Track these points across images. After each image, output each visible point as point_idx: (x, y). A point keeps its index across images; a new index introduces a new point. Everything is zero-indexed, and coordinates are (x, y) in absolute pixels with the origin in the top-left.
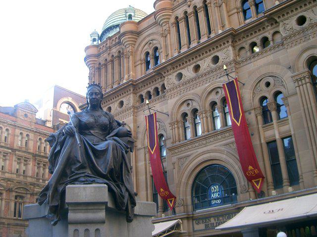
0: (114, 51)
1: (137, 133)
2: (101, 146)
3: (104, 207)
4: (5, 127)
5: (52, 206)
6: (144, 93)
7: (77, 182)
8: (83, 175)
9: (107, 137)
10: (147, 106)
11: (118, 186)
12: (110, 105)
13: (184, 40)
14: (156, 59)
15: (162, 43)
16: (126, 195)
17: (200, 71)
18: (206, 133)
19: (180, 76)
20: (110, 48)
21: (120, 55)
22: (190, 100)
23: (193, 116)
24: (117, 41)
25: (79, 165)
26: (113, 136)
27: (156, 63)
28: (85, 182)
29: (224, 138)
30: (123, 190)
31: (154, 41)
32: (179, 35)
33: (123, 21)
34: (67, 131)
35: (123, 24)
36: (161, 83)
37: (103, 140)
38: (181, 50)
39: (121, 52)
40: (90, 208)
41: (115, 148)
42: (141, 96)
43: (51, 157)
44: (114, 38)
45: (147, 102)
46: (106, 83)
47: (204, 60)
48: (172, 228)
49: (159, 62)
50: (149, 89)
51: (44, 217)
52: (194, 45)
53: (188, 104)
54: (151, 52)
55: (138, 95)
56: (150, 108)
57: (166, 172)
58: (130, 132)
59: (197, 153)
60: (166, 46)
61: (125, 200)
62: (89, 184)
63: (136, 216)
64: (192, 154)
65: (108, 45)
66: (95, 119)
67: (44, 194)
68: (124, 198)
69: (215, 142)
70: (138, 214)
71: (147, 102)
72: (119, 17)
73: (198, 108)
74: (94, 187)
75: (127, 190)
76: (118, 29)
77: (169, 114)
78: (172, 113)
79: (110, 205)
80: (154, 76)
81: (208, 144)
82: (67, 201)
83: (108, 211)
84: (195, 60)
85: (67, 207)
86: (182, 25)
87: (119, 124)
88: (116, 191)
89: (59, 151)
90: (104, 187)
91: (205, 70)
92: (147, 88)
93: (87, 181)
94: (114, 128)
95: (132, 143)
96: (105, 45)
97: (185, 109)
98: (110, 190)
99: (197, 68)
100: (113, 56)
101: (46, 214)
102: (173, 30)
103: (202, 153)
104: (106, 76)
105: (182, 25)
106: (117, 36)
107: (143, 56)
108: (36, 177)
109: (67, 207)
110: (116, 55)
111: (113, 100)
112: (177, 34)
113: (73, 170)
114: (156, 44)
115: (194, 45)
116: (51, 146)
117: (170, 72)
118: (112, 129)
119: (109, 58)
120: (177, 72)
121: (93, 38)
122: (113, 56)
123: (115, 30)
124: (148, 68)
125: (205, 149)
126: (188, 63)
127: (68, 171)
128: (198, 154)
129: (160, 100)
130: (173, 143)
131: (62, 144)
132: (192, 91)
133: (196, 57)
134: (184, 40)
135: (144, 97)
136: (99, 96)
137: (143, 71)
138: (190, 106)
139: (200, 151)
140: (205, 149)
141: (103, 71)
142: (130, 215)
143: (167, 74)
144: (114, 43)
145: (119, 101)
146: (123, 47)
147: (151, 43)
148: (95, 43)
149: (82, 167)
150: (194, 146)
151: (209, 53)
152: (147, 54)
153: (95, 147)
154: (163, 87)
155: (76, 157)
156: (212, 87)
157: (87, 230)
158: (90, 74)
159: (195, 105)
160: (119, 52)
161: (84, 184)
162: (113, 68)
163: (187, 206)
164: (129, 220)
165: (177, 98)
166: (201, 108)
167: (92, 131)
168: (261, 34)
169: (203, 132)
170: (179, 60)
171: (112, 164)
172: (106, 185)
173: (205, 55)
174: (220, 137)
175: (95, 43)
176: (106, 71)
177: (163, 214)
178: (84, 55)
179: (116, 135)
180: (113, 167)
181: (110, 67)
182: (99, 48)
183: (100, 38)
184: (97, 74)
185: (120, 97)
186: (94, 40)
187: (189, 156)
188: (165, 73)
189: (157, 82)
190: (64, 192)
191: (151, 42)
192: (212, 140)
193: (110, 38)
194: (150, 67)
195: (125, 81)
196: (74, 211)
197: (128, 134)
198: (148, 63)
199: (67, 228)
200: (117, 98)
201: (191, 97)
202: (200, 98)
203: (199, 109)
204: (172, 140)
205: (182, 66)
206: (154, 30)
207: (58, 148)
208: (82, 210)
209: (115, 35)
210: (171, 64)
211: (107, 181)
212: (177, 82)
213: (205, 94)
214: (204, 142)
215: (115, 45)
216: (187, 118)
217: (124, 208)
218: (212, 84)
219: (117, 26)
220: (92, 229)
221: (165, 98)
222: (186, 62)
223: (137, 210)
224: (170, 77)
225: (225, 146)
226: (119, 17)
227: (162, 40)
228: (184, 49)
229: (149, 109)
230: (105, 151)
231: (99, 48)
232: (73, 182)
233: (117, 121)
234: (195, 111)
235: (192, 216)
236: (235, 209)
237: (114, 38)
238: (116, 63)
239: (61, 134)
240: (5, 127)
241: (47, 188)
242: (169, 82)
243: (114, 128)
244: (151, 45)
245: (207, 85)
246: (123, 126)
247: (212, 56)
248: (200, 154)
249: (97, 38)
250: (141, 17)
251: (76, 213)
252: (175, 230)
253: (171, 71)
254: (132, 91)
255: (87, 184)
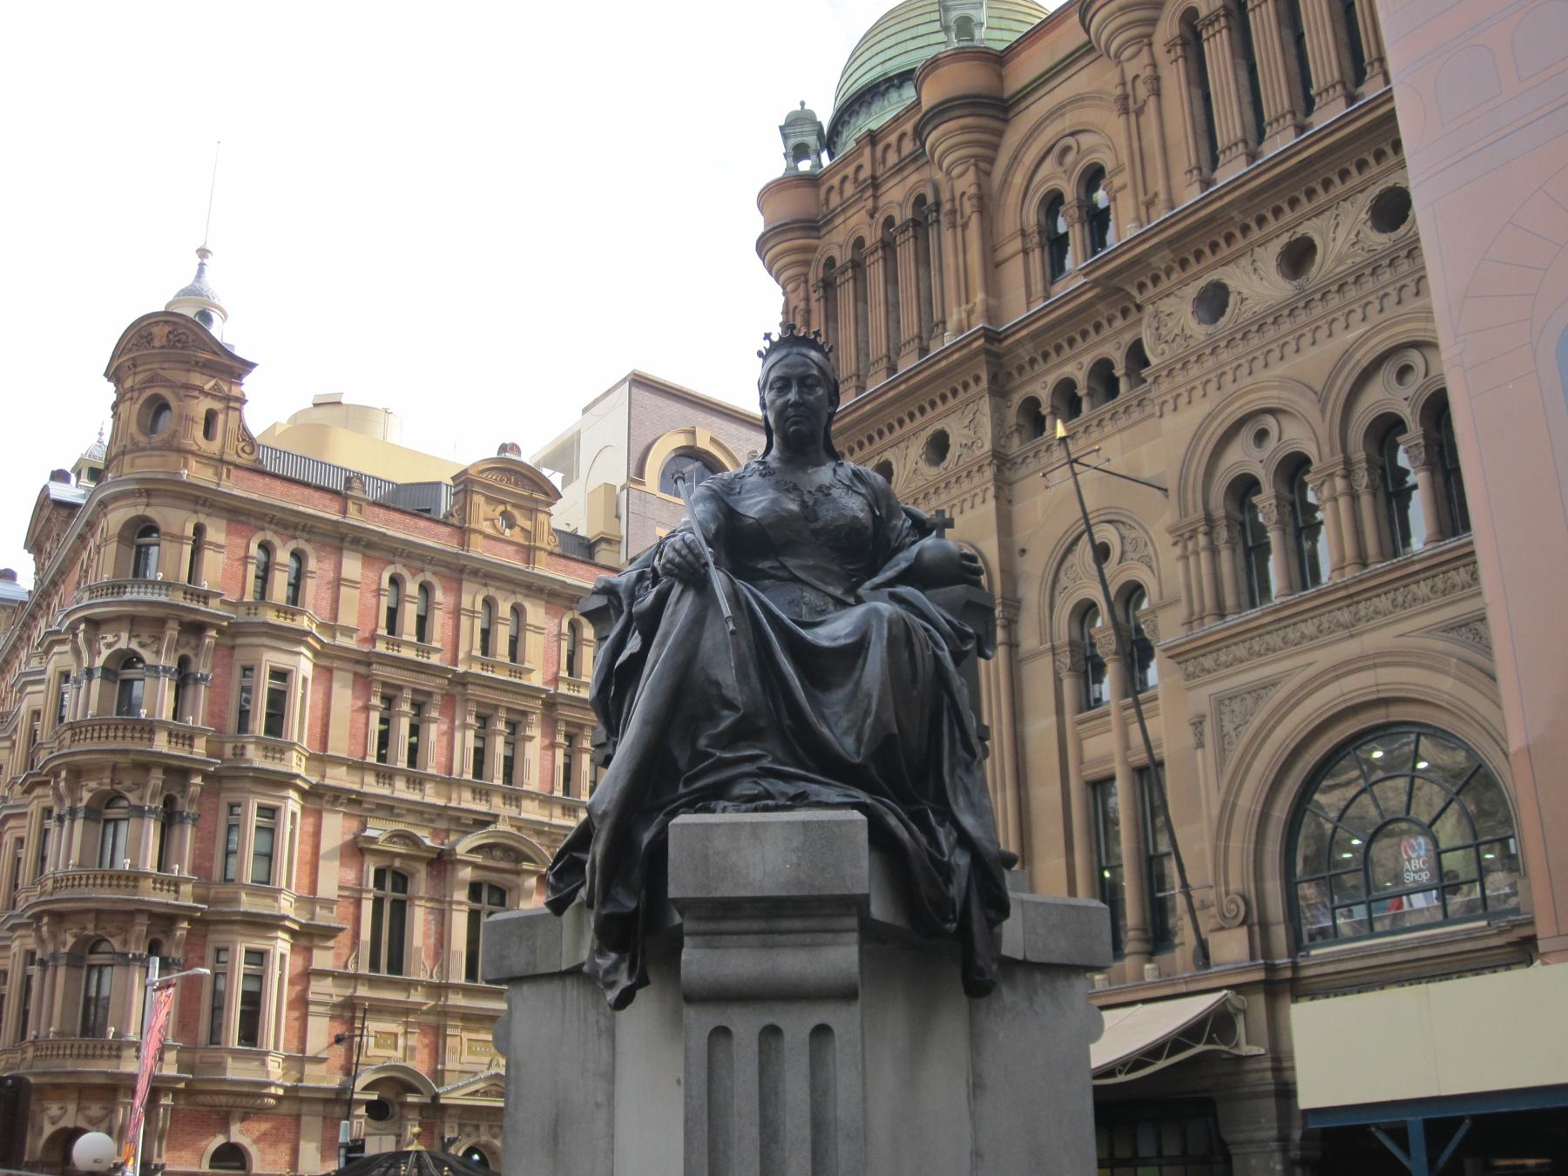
0: (896, 196)
1: (1010, 575)
2: (836, 630)
3: (853, 922)
4: (414, 575)
5: (607, 916)
6: (1042, 389)
7: (722, 804)
8: (747, 768)
9: (861, 591)
10: (1059, 454)
11: (920, 820)
12: (889, 455)
13: (1230, 123)
14: (1097, 221)
15: (1121, 141)
16: (962, 860)
17: (1314, 269)
18: (1351, 573)
19: (1214, 301)
20: (875, 184)
21: (924, 217)
22: (1272, 411)
23: (1286, 493)
24: (908, 146)
25: (728, 719)
26: (891, 583)
27: (1098, 240)
28: (754, 802)
29: (1444, 593)
30: (944, 836)
31: (1082, 138)
32: (1207, 98)
33: (930, 53)
34: (670, 561)
35: (934, 64)
36: (1127, 338)
37: (841, 604)
38: (1218, 174)
39: (930, 199)
40: (786, 924)
41: (901, 639)
42: (1031, 405)
43: (603, 688)
44: (893, 138)
45: (1060, 431)
46: (862, 349)
47: (1333, 211)
48: (1191, 1033)
49: (1111, 238)
50: (1069, 370)
51: (575, 972)
52: (1280, 141)
53: (1261, 436)
54: (1070, 192)
55: (1017, 399)
56: (1075, 461)
57: (1160, 764)
58: (973, 559)
59: (1311, 671)
60: (1140, 158)
61: (956, 890)
62: (778, 808)
63: (1012, 966)
64: (1289, 673)
65: (866, 173)
66: (804, 504)
67: (568, 866)
68: (948, 880)
69: (1400, 613)
70: (1020, 957)
71: (1060, 431)
72: (914, 32)
73: (1311, 450)
74: (806, 825)
75: (964, 840)
76: (909, 93)
77: (1171, 484)
78: (1182, 477)
79: (879, 910)
80: (1090, 304)
81: (1362, 626)
82: (673, 892)
83: (870, 932)
84: (1288, 216)
85: (677, 919)
86: (1218, 50)
87: (921, 527)
88: (905, 835)
89: (639, 659)
90: (851, 822)
91: (1340, 260)
92: (1062, 364)
93: (769, 796)
94: (895, 544)
95: (980, 611)
96: (850, 171)
97: (1243, 457)
98: (880, 836)
99: (1298, 257)
100: (889, 222)
101: (585, 955)
102: (1174, 77)
103: (1334, 667)
104: (861, 320)
105: (1218, 50)
106: (908, 127)
107: (1032, 216)
108: (558, 793)
109: (677, 919)
110: (902, 215)
111: (898, 432)
112: (1197, 93)
113: (702, 742)
114: (1091, 150)
115: (1280, 141)
116: (601, 639)
117: (1165, 284)
118: (888, 551)
119: (872, 236)
120: (1202, 283)
121: (793, 142)
122: (889, 222)
123: (893, 95)
124: (1056, 268)
125: (1350, 648)
126: (1256, 234)
127: (682, 757)
128: (1316, 677)
129: (1122, 422)
130: (1189, 623)
131: (649, 623)
132: (1279, 370)
133: (1294, 203)
134: (1230, 123)
135: (1045, 410)
136: (820, 391)
137: (1038, 287)
138: (1271, 443)
139: (1324, 657)
140: (1350, 648)
141: (846, 294)
142: (980, 963)
143: (1151, 290)
144: (892, 158)
145: (929, 431)
146: (939, 176)
147: (1067, 149)
148: (805, 166)
149: (743, 732)
150: (1292, 635)
151: (1355, 179)
152: (1053, 202)
153: (807, 634)
154: (1137, 357)
155: (717, 684)
156: (1378, 344)
157: (722, 1032)
158: (786, 312)
159: (1295, 436)
160: (920, 200)
161: (756, 810)
162: (891, 279)
163: (1265, 926)
164: (978, 988)
165: (1202, 408)
166: (1326, 449)
167: (791, 563)
168: (1057, 366)
169: (1339, 568)
170: (1211, 218)
171: (889, 715)
172: (857, 815)
173: (1338, 188)
174: (1423, 589)
175: (805, 166)
176: (861, 297)
177: (1147, 966)
178: (757, 225)
179: (914, 575)
180: (895, 730)
181: (876, 273)
182: (823, 190)
183: (829, 141)
184: (817, 308)
185: (930, 414)
186: (799, 152)
187: (1271, 684)
188: (1142, 287)
189: (1106, 331)
190: (660, 847)
191: (1070, 141)
192: (1383, 603)
193: (873, 138)
194: (1069, 262)
195: (949, 340)
196: (711, 938)
197: (964, 569)
198: (1057, 246)
199: (264, 1063)
200: (919, 420)
201: (1271, 398)
202: (1322, 400)
203: (1313, 455)
204: (1181, 612)
205: (1225, 251)
206: (1080, 81)
207: (634, 644)
208: (747, 933)
209: (896, 119)
210: (1169, 242)
211: (863, 797)
212: (1199, 331)
213: (1344, 383)
214: (1345, 616)
215: (899, 169)
216: (1255, 499)
217: (952, 927)
218: (1376, 330)
219: (905, 77)
220: (796, 1024)
221: (1148, 410)
222: (1245, 229)
223: (1014, 937)
224: (1166, 305)
225: (1453, 635)
226: (914, 32)
227: (1115, 124)
228: (1231, 170)
229: (1072, 462)
230: (855, 651)
231: (823, 190)
232: (702, 801)
233: (909, 514)
234: (1294, 468)
235: (1288, 974)
236: (1510, 944)
237: (893, 138)
238: (906, 253)
239: (647, 576)
240: (414, 575)
241: (583, 837)
242: (1163, 331)
243: (895, 544)
244: (1070, 157)
245: (1350, 336)
246: (941, 535)
247: (1375, 191)
248: (1324, 672)
249: (812, 140)
250: (1014, 25)
251: (771, 947)
252: (1210, 1041)
253: (1174, 276)
254: (984, 383)
255: (766, 809)
